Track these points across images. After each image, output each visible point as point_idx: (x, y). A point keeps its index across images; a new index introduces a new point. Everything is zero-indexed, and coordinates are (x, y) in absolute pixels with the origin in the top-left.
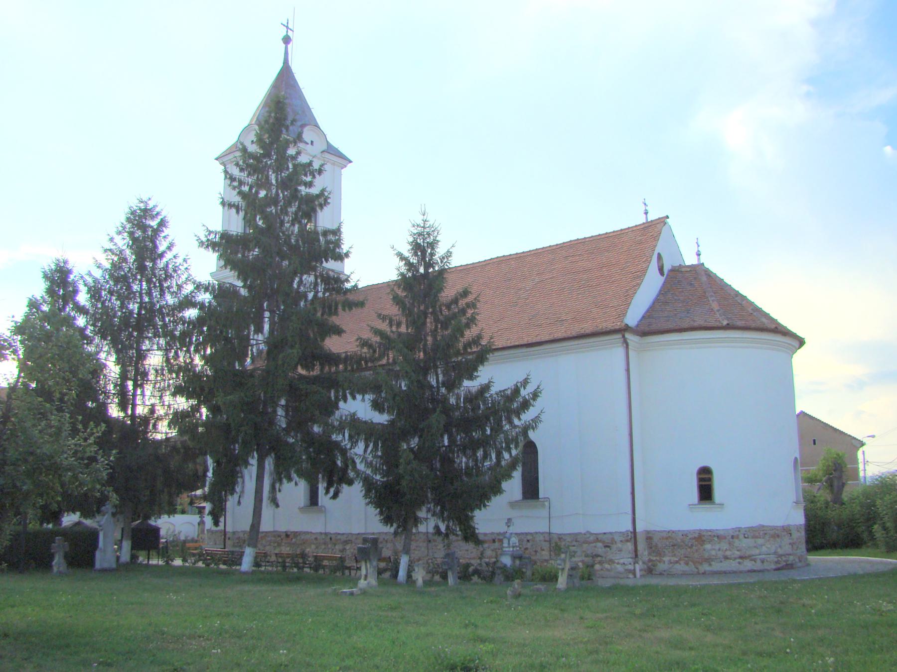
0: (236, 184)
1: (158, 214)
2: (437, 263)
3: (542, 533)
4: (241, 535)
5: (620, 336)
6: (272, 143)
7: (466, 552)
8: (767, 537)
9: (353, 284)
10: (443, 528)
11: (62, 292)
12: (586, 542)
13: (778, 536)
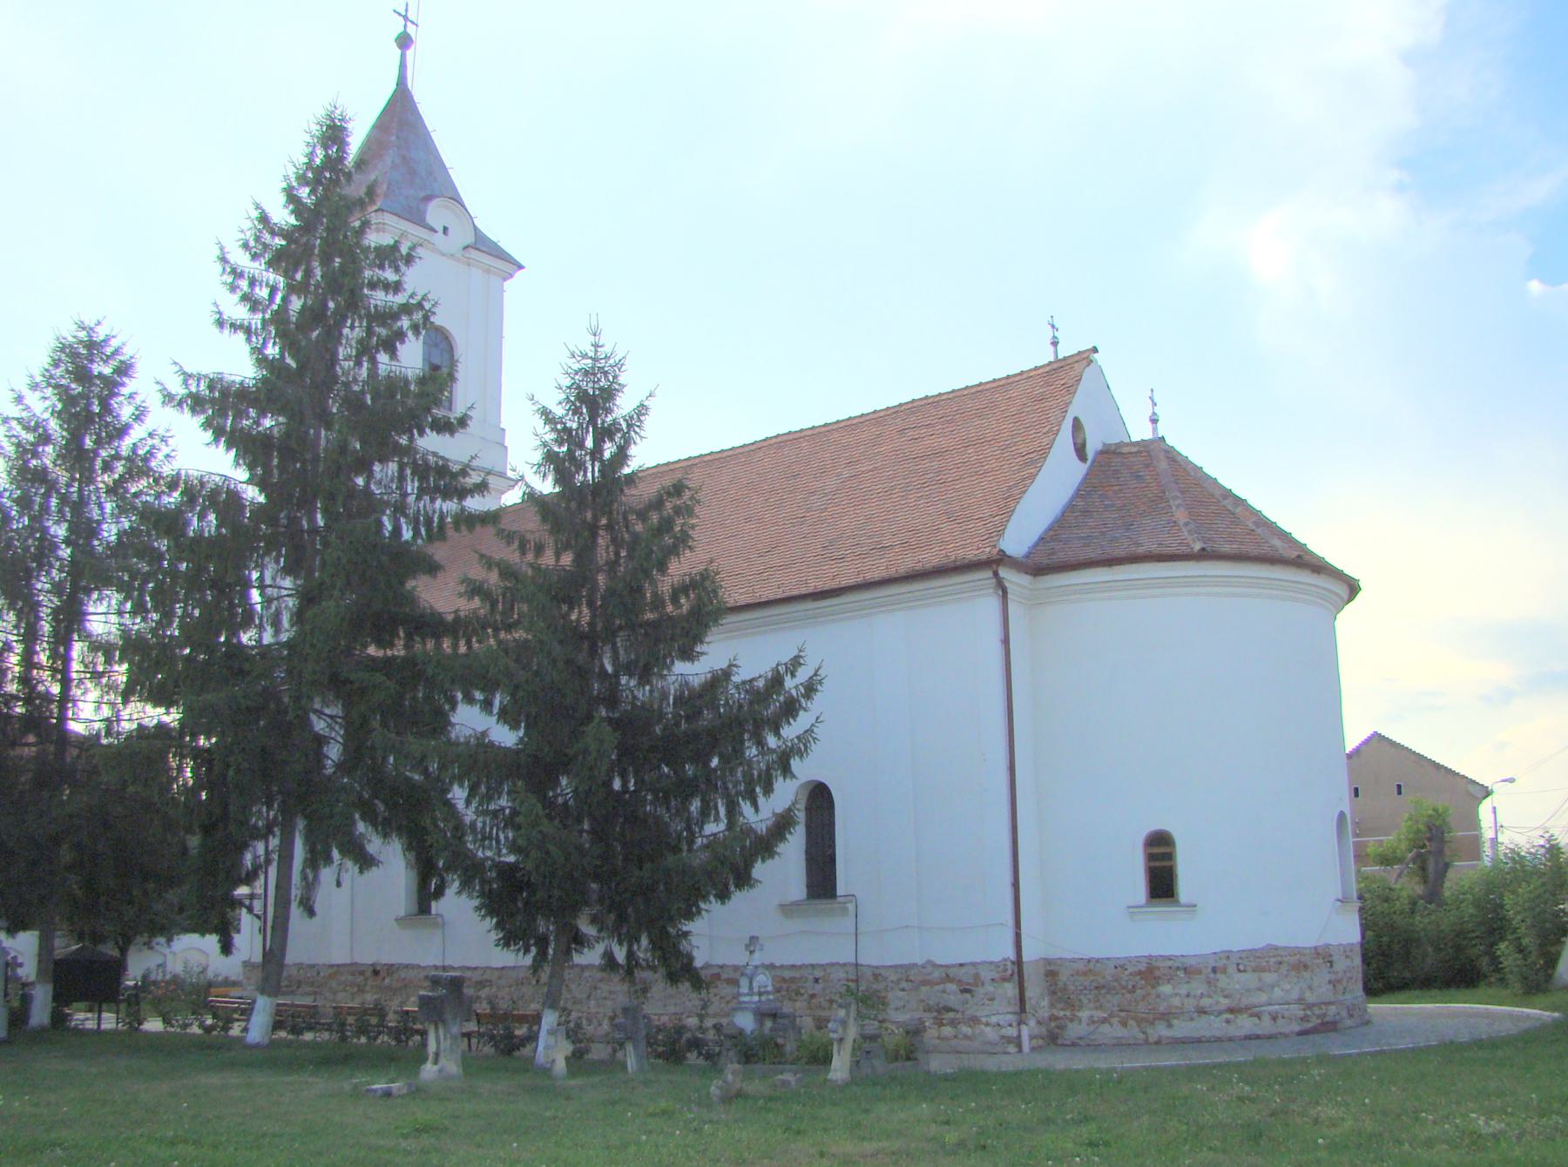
1: (117, 352)
5: (989, 574)
7: (667, 1004)
8: (1284, 968)
10: (620, 955)
12: (925, 983)
13: (1306, 967)
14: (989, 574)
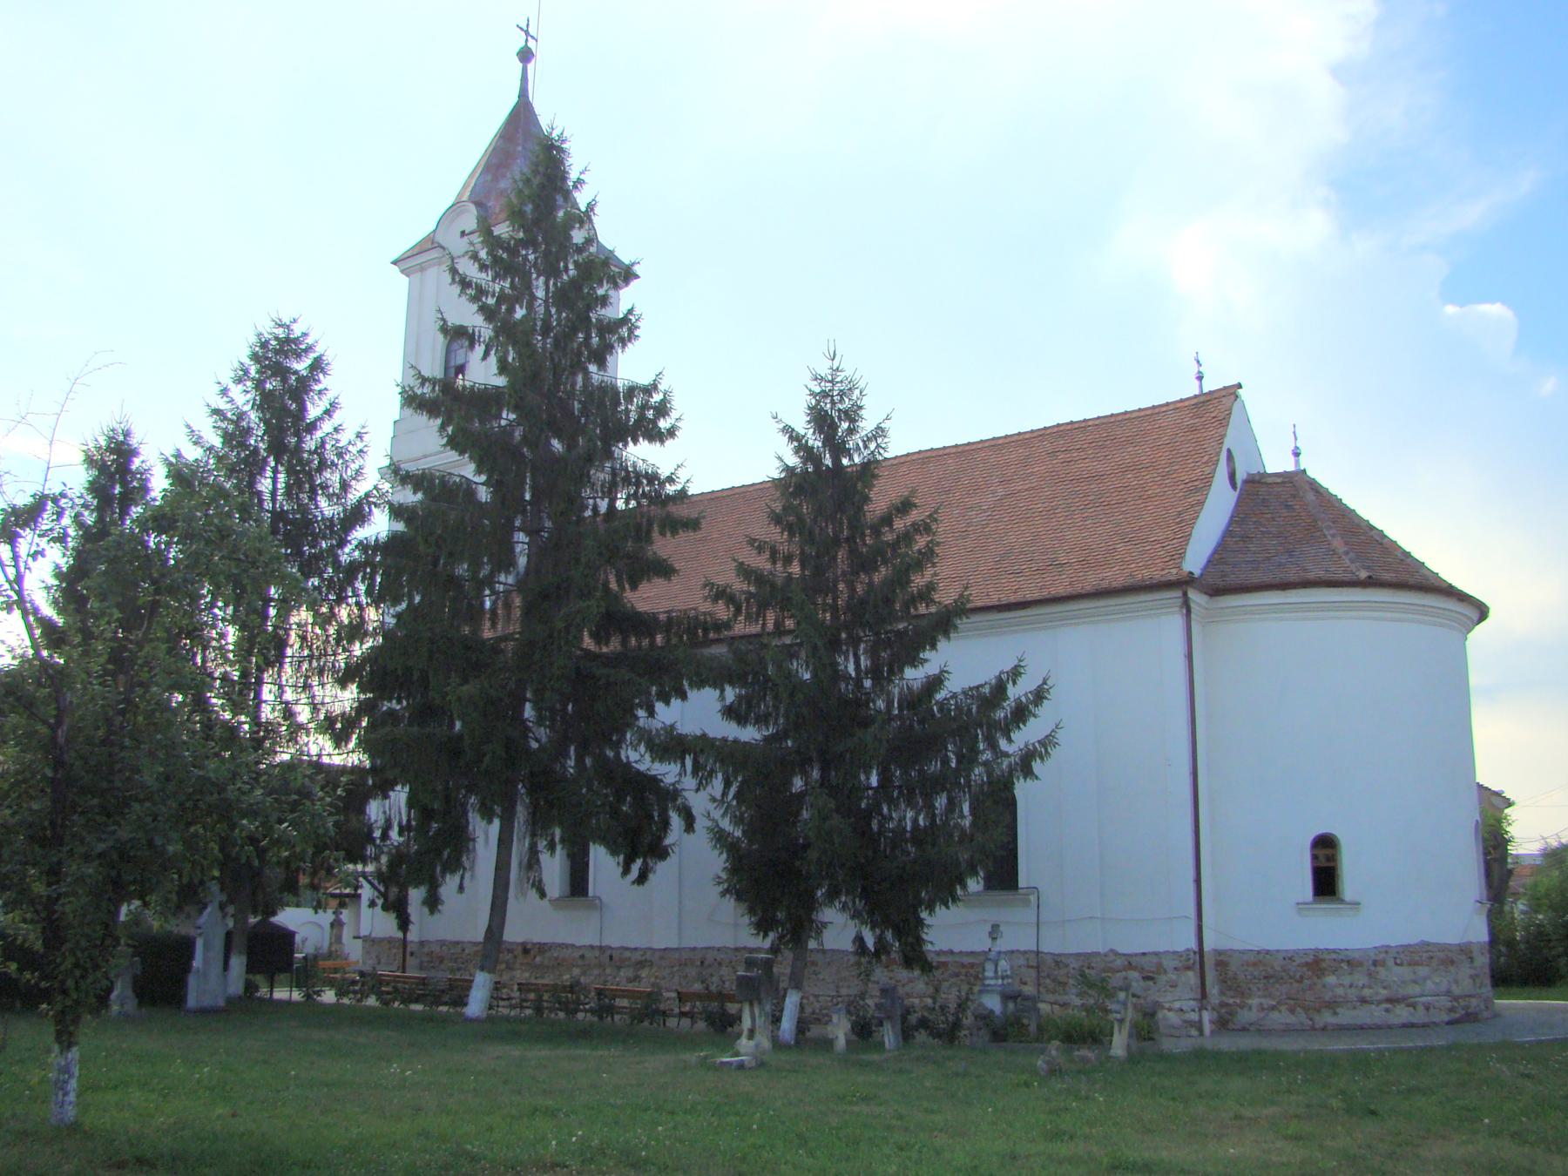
0: (471, 292)
2: (858, 448)
3: (1025, 952)
4: (436, 949)
5: (1179, 593)
6: (537, 222)
7: (915, 988)
9: (679, 487)
10: (870, 941)
11: (118, 489)
13: (1452, 962)
14: (1179, 593)
